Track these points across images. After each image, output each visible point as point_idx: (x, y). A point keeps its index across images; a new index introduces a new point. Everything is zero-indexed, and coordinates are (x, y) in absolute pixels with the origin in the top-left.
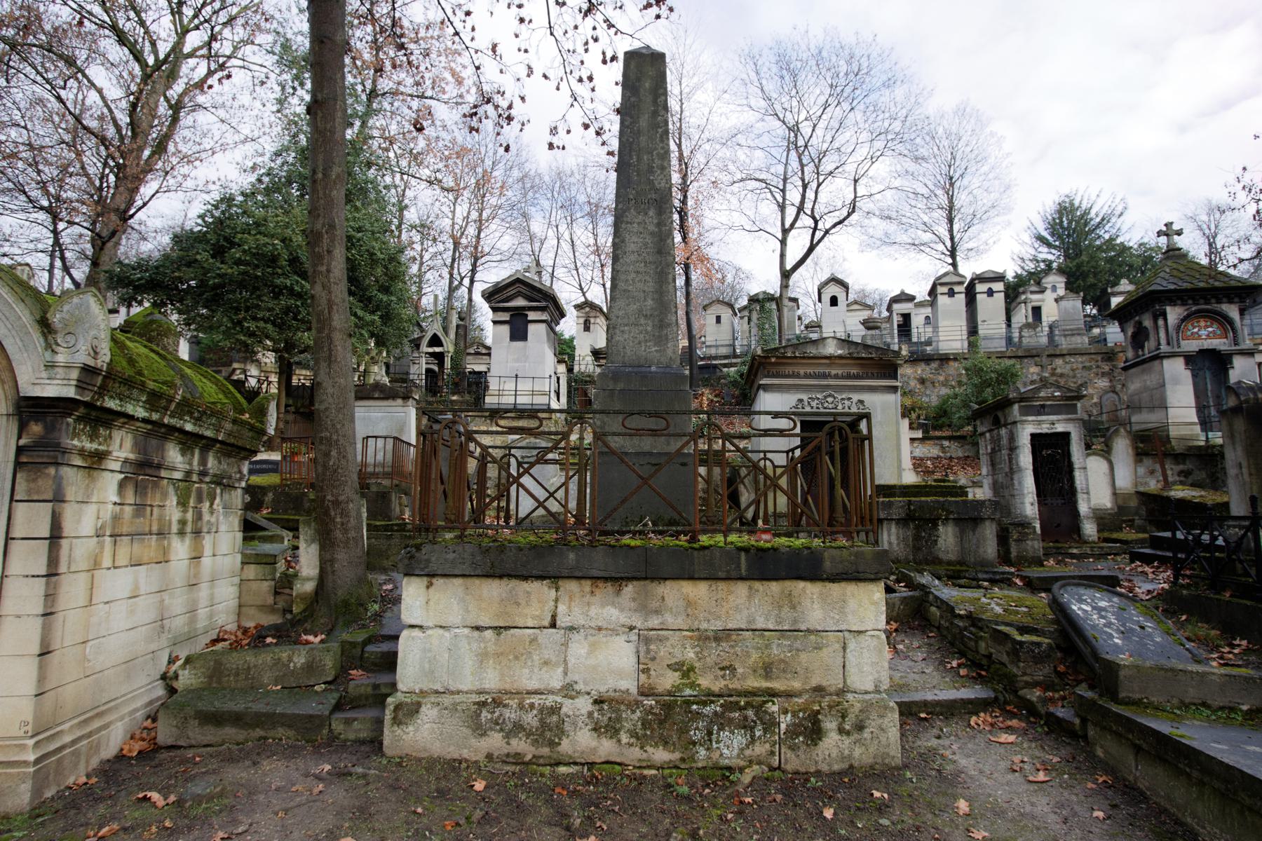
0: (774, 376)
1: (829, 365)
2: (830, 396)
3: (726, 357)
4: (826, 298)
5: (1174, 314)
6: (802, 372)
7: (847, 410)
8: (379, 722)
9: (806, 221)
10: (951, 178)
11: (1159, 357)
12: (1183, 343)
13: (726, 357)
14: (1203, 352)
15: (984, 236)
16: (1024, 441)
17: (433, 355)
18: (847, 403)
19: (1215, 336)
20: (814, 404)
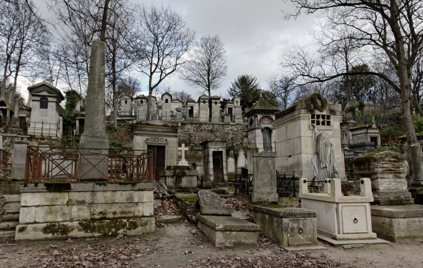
0: (141, 130)
1: (157, 128)
2: (157, 137)
3: (128, 116)
4: (164, 99)
5: (259, 116)
6: (148, 130)
7: (162, 142)
8: (15, 233)
9: (158, 70)
10: (210, 61)
11: (255, 129)
12: (261, 125)
13: (128, 116)
14: (266, 128)
15: (218, 82)
16: (211, 153)
18: (161, 141)
19: (268, 123)
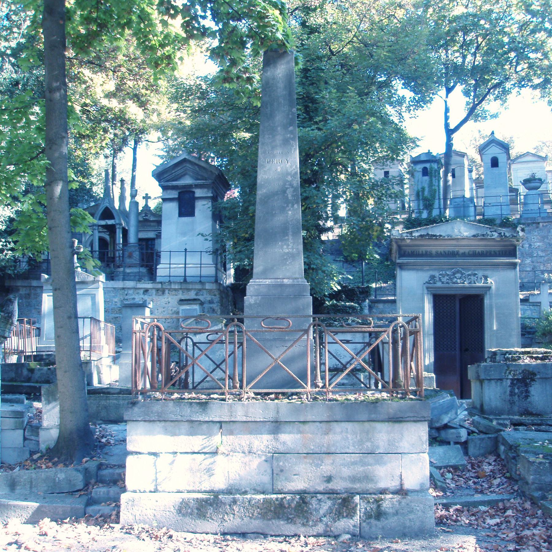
2: (458, 272)
17: (106, 227)
20: (444, 280)
